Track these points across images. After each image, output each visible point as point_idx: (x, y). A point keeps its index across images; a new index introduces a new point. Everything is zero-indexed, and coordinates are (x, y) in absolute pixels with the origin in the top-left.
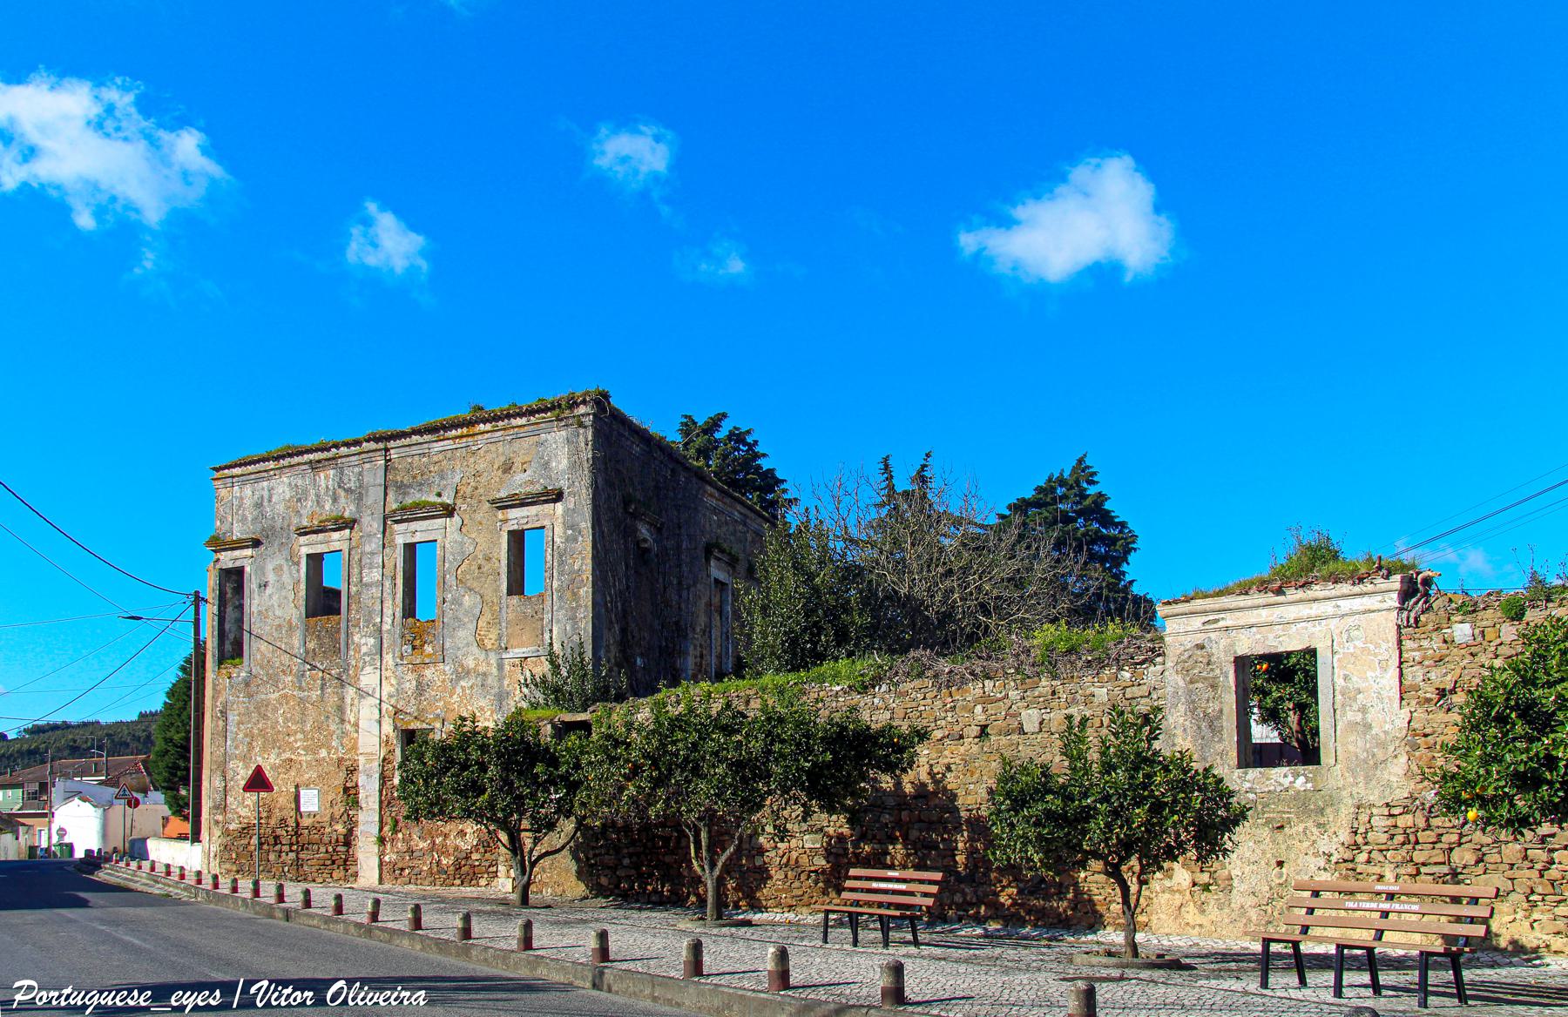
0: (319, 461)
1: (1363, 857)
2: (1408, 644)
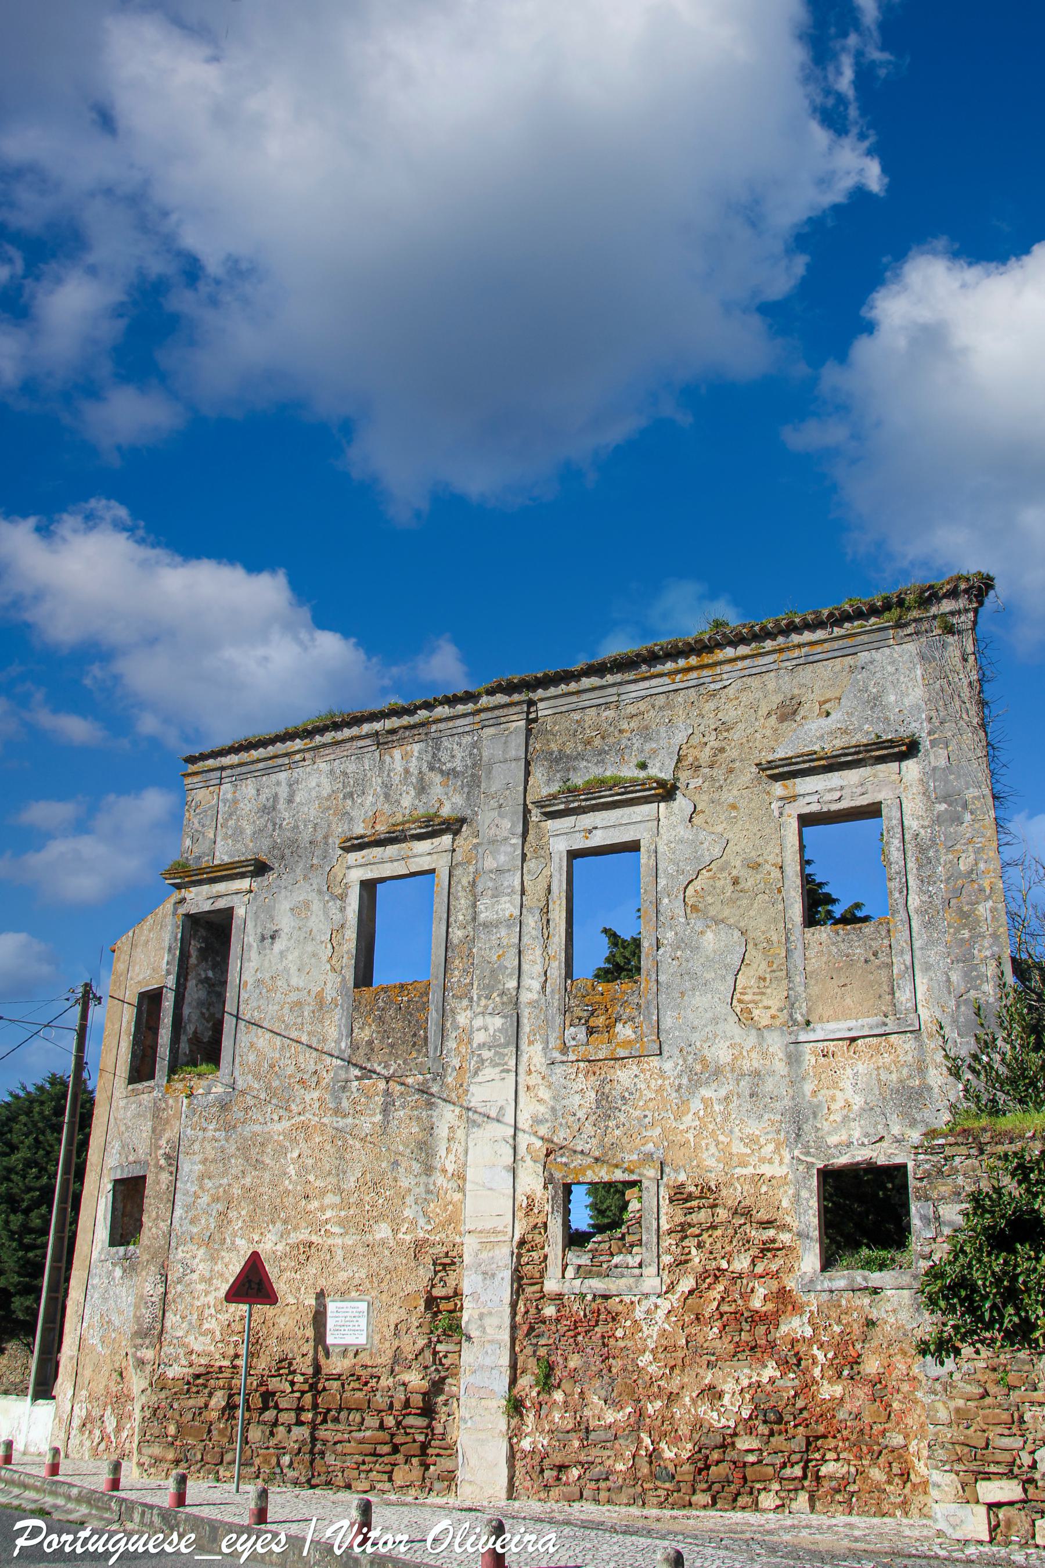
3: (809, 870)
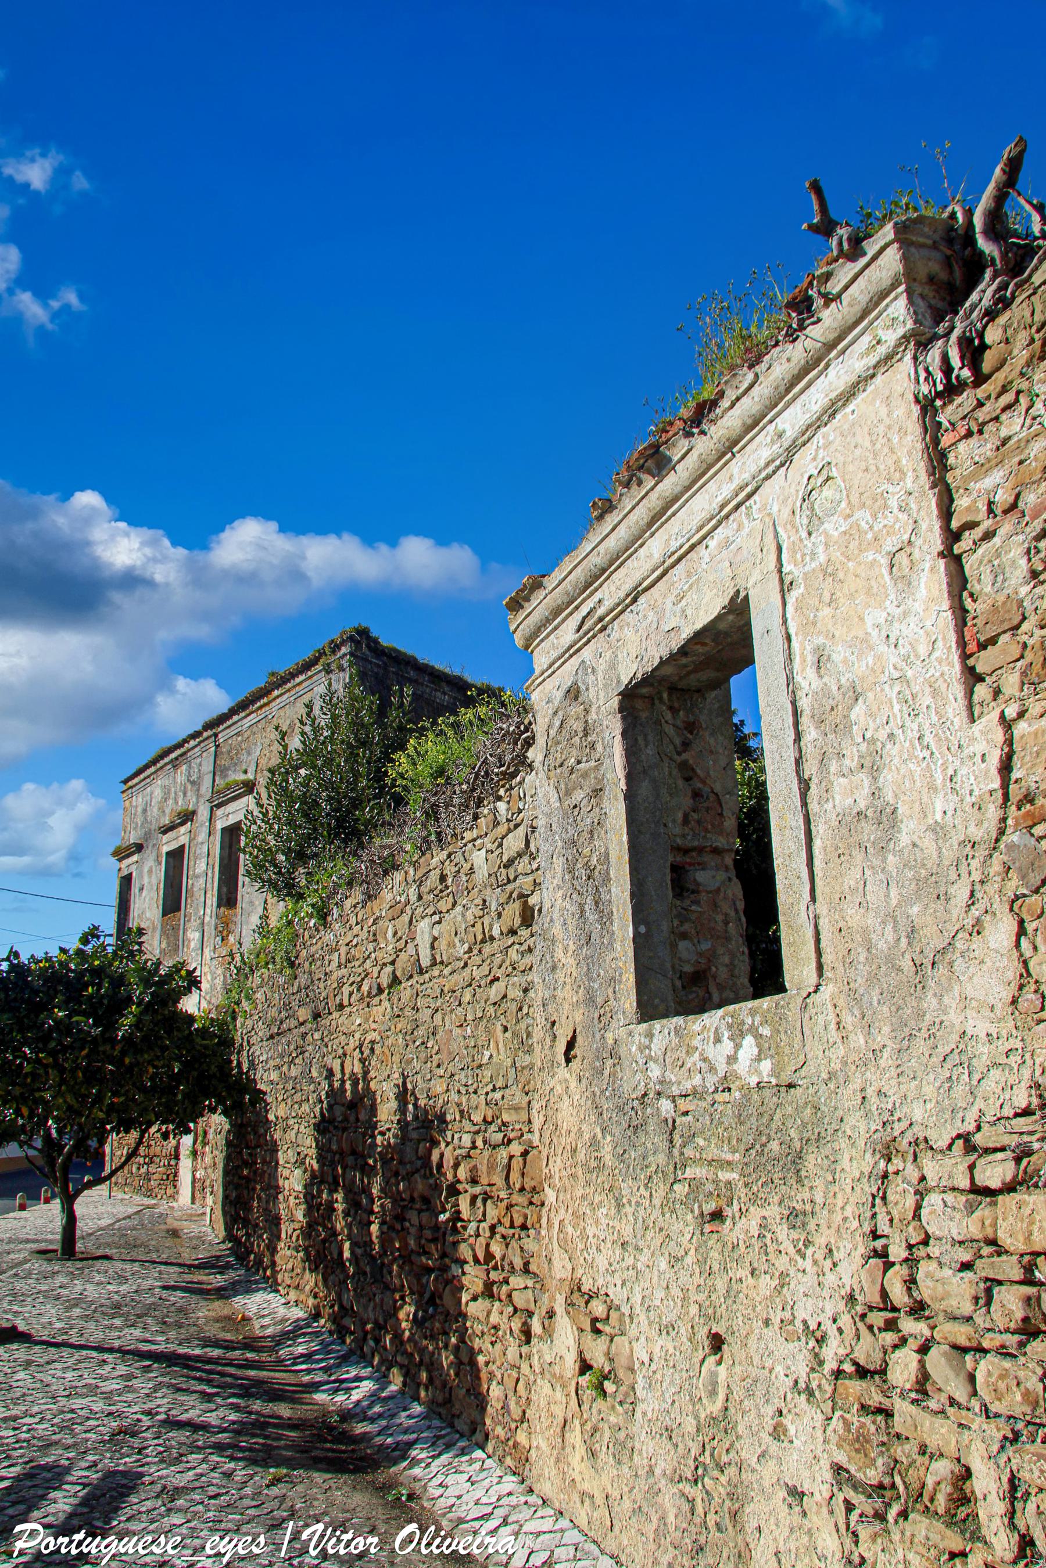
0: (177, 759)
1: (903, 1368)
2: (964, 455)
3: (971, 662)
